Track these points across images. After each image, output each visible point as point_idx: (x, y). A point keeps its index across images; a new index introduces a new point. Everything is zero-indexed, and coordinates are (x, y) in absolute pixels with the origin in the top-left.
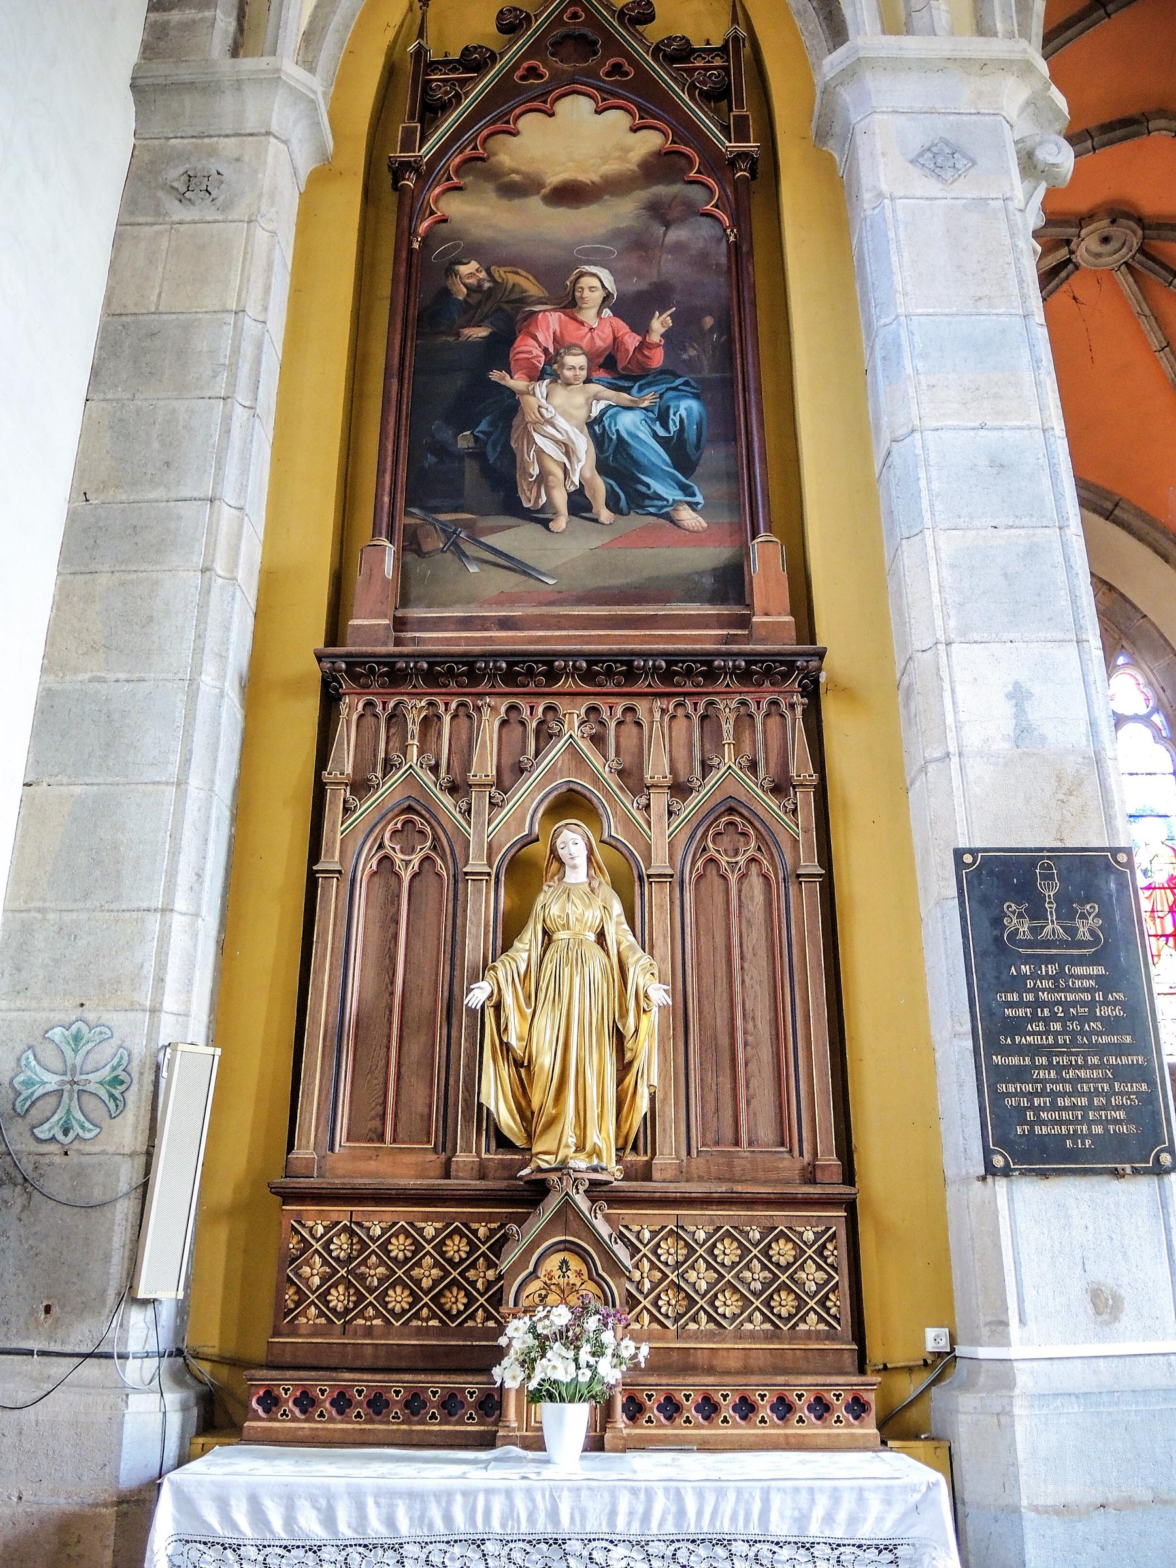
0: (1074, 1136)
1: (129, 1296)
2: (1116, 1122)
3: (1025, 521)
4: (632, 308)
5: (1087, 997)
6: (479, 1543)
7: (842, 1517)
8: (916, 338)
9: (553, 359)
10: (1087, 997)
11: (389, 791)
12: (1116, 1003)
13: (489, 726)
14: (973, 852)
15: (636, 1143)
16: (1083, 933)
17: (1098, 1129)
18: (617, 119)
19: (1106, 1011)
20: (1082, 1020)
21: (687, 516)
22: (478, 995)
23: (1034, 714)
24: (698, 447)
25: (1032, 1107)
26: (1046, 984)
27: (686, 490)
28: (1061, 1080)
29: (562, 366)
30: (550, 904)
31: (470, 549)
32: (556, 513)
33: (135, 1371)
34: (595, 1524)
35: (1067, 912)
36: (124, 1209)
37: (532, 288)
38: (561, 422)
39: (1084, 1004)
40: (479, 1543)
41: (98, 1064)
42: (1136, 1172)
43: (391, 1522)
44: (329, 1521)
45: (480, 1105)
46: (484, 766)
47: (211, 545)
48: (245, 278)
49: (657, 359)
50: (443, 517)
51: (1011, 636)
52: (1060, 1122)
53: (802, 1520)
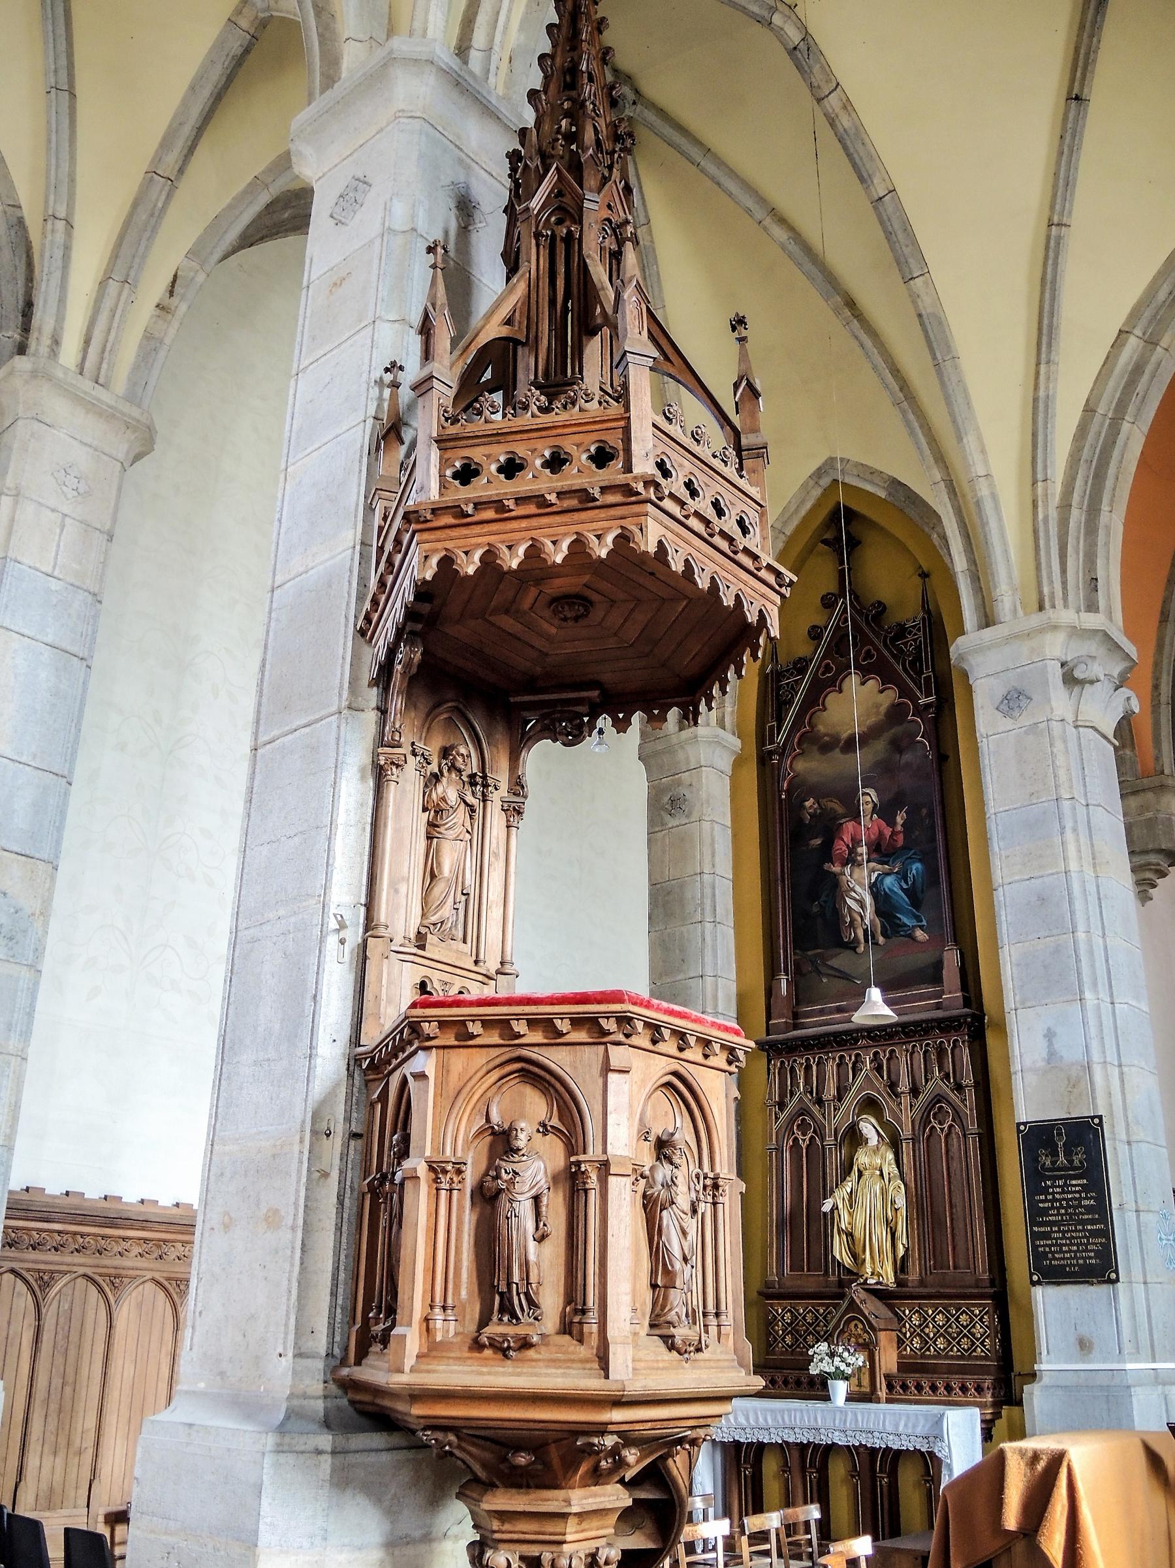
0: (1070, 1265)
2: (1090, 1258)
3: (1055, 932)
4: (885, 811)
5: (1077, 1195)
6: (793, 1429)
7: (910, 1425)
8: (1000, 828)
9: (852, 850)
10: (1077, 1195)
12: (1092, 1198)
13: (831, 1068)
14: (1025, 1124)
15: (901, 1267)
16: (1076, 1163)
17: (1081, 1262)
18: (872, 684)
19: (1086, 1202)
20: (1075, 1207)
21: (920, 934)
22: (827, 1207)
23: (1058, 1045)
24: (922, 892)
25: (1051, 1252)
26: (1059, 1190)
27: (919, 920)
28: (1064, 1238)
29: (856, 854)
30: (862, 1158)
31: (823, 969)
32: (859, 943)
34: (829, 1424)
35: (1068, 1154)
37: (840, 809)
38: (859, 886)
39: (1076, 1199)
40: (793, 1429)
42: (1099, 1282)
43: (766, 1420)
44: (747, 1419)
45: (834, 1257)
46: (831, 1091)
47: (704, 1000)
48: (701, 854)
49: (900, 840)
50: (810, 953)
51: (1047, 1001)
52: (1063, 1259)
53: (897, 1426)
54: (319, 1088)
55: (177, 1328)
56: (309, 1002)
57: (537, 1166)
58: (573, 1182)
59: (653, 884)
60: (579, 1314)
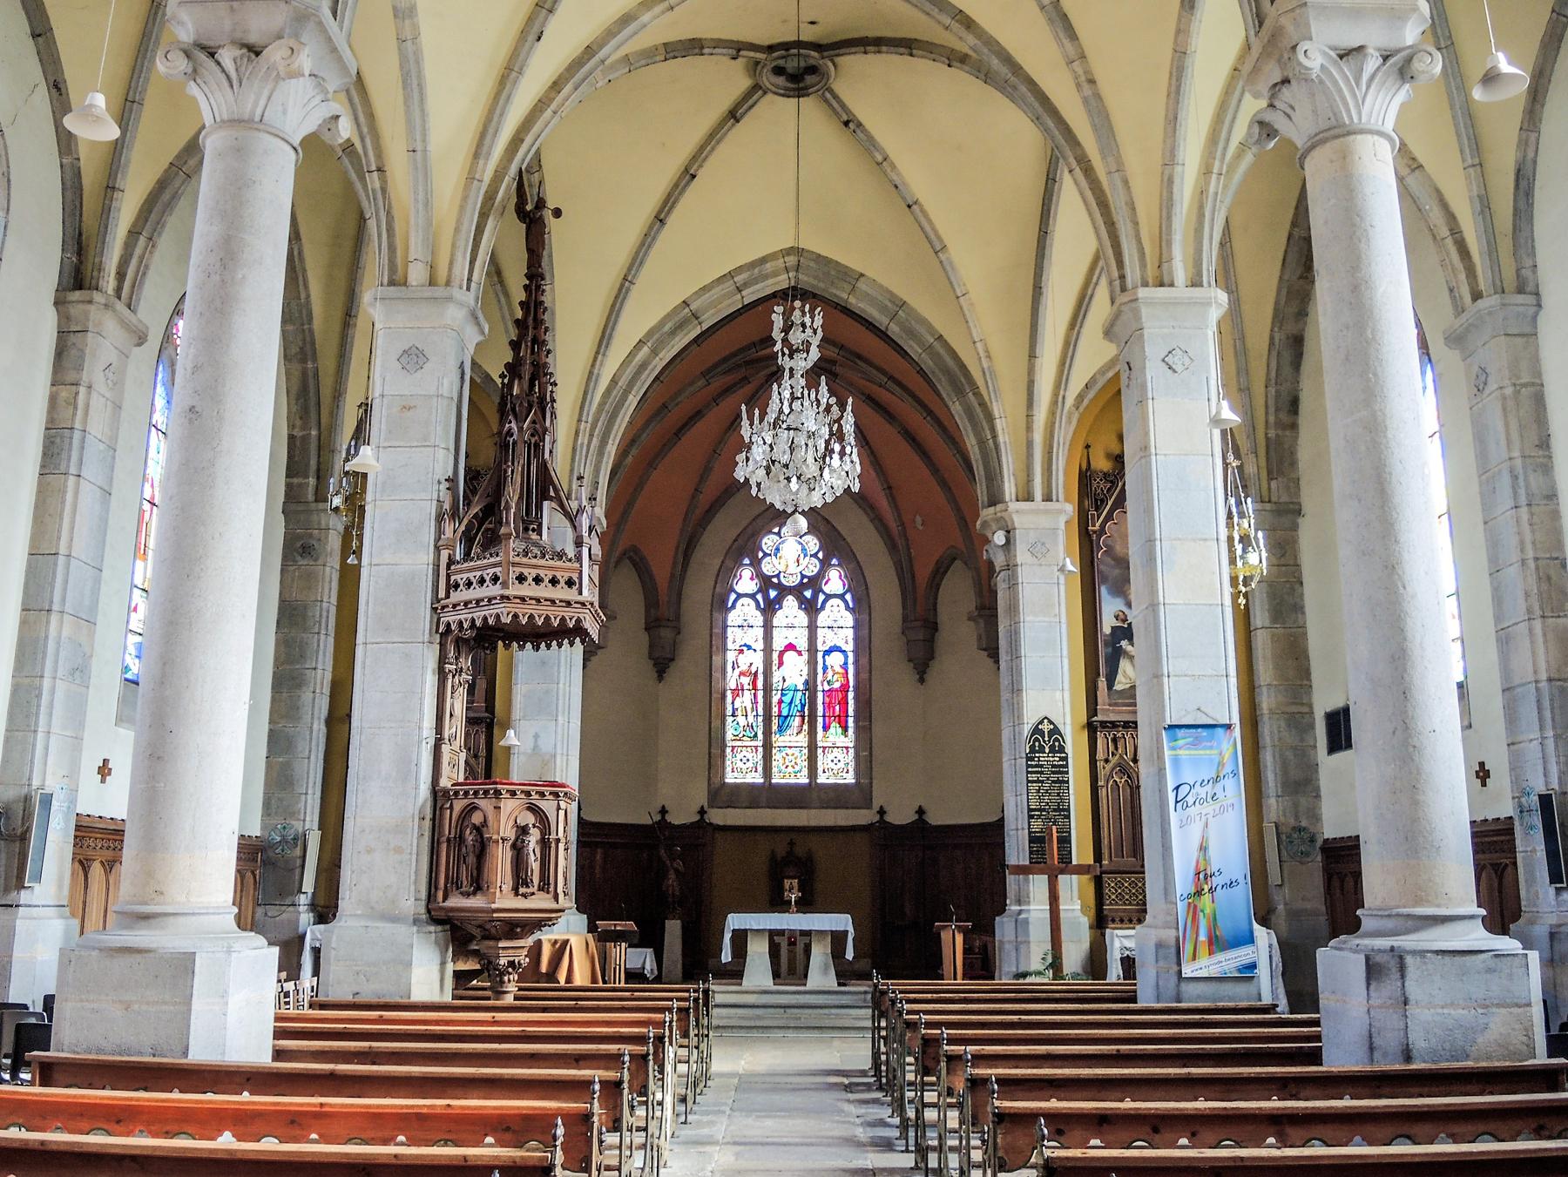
1: (300, 891)
11: (1114, 760)
33: (302, 909)
36: (298, 871)
41: (291, 835)
54: (421, 800)
55: (86, 887)
56: (413, 768)
57: (534, 837)
58: (544, 843)
59: (282, 601)
60: (544, 886)
